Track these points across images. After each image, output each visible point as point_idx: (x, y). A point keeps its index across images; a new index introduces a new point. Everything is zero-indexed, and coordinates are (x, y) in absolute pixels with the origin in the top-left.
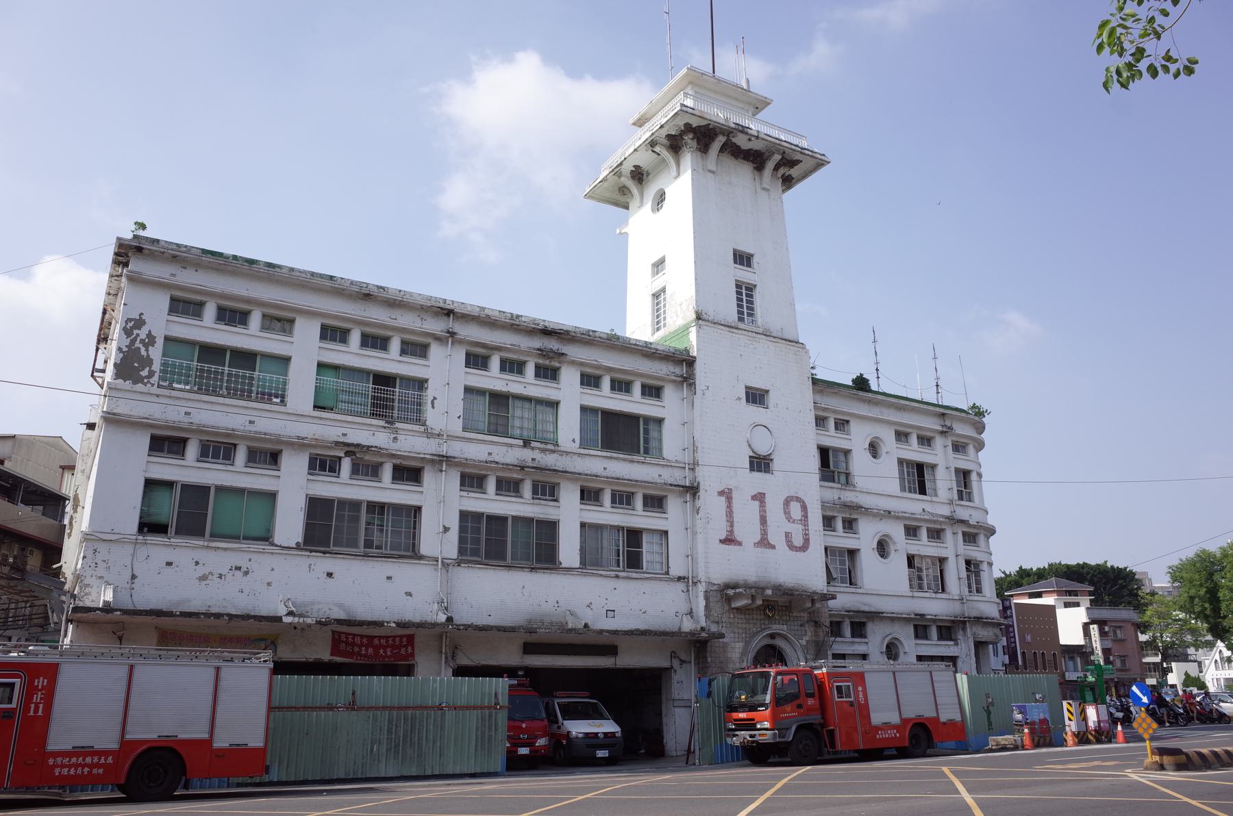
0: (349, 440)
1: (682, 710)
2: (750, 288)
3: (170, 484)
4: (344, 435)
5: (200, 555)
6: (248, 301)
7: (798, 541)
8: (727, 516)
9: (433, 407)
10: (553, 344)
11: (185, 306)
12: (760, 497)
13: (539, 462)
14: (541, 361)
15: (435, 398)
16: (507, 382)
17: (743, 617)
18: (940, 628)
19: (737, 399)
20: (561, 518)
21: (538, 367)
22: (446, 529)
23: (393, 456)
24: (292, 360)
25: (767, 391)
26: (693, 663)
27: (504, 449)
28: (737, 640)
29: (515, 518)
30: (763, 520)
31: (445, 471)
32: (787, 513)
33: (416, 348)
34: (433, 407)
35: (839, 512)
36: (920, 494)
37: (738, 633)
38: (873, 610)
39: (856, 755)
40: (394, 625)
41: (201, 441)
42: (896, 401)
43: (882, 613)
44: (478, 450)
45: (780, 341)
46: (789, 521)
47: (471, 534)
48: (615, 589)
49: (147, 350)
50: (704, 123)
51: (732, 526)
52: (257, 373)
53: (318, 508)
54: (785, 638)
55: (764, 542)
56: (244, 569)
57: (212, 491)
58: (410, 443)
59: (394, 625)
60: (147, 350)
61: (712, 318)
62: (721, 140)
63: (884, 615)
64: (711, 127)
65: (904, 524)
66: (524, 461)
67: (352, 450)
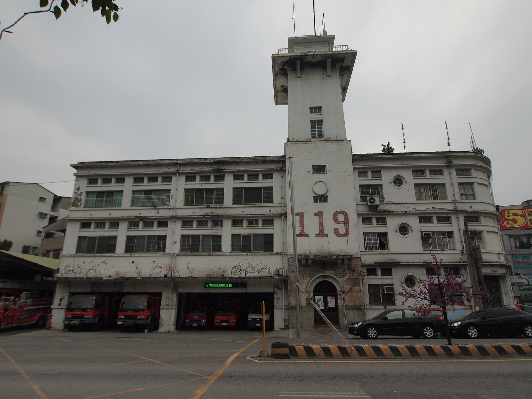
0: (142, 215)
1: (279, 310)
2: (320, 122)
3: (86, 237)
4: (140, 214)
5: (155, 259)
6: (110, 175)
7: (342, 231)
8: (300, 224)
9: (172, 199)
10: (218, 167)
11: (92, 180)
12: (320, 214)
13: (214, 213)
14: (216, 174)
15: (173, 196)
16: (201, 185)
17: (309, 268)
18: (382, 270)
19: (307, 172)
20: (223, 233)
21: (215, 176)
22: (175, 242)
23: (195, 218)
24: (124, 191)
25: (325, 166)
26: (284, 289)
27: (199, 210)
28: (305, 279)
29: (203, 236)
30: (321, 224)
31: (174, 221)
32: (336, 220)
33: (167, 178)
34: (172, 199)
35: (373, 215)
36: (433, 200)
37: (306, 276)
38: (395, 261)
39: (280, 329)
40: (140, 279)
41: (157, 221)
42: (431, 155)
43: (400, 263)
44: (188, 212)
45: (333, 141)
46: (337, 223)
47: (187, 243)
48: (247, 260)
49: (80, 197)
50: (288, 58)
51: (303, 228)
52: (114, 198)
53: (130, 240)
54: (330, 277)
55: (322, 234)
56: (106, 263)
57: (201, 237)
58: (164, 213)
59: (140, 279)
60: (80, 197)
61: (297, 140)
62: (298, 62)
63: (401, 264)
64: (292, 59)
65: (419, 217)
66: (208, 213)
67: (142, 219)
